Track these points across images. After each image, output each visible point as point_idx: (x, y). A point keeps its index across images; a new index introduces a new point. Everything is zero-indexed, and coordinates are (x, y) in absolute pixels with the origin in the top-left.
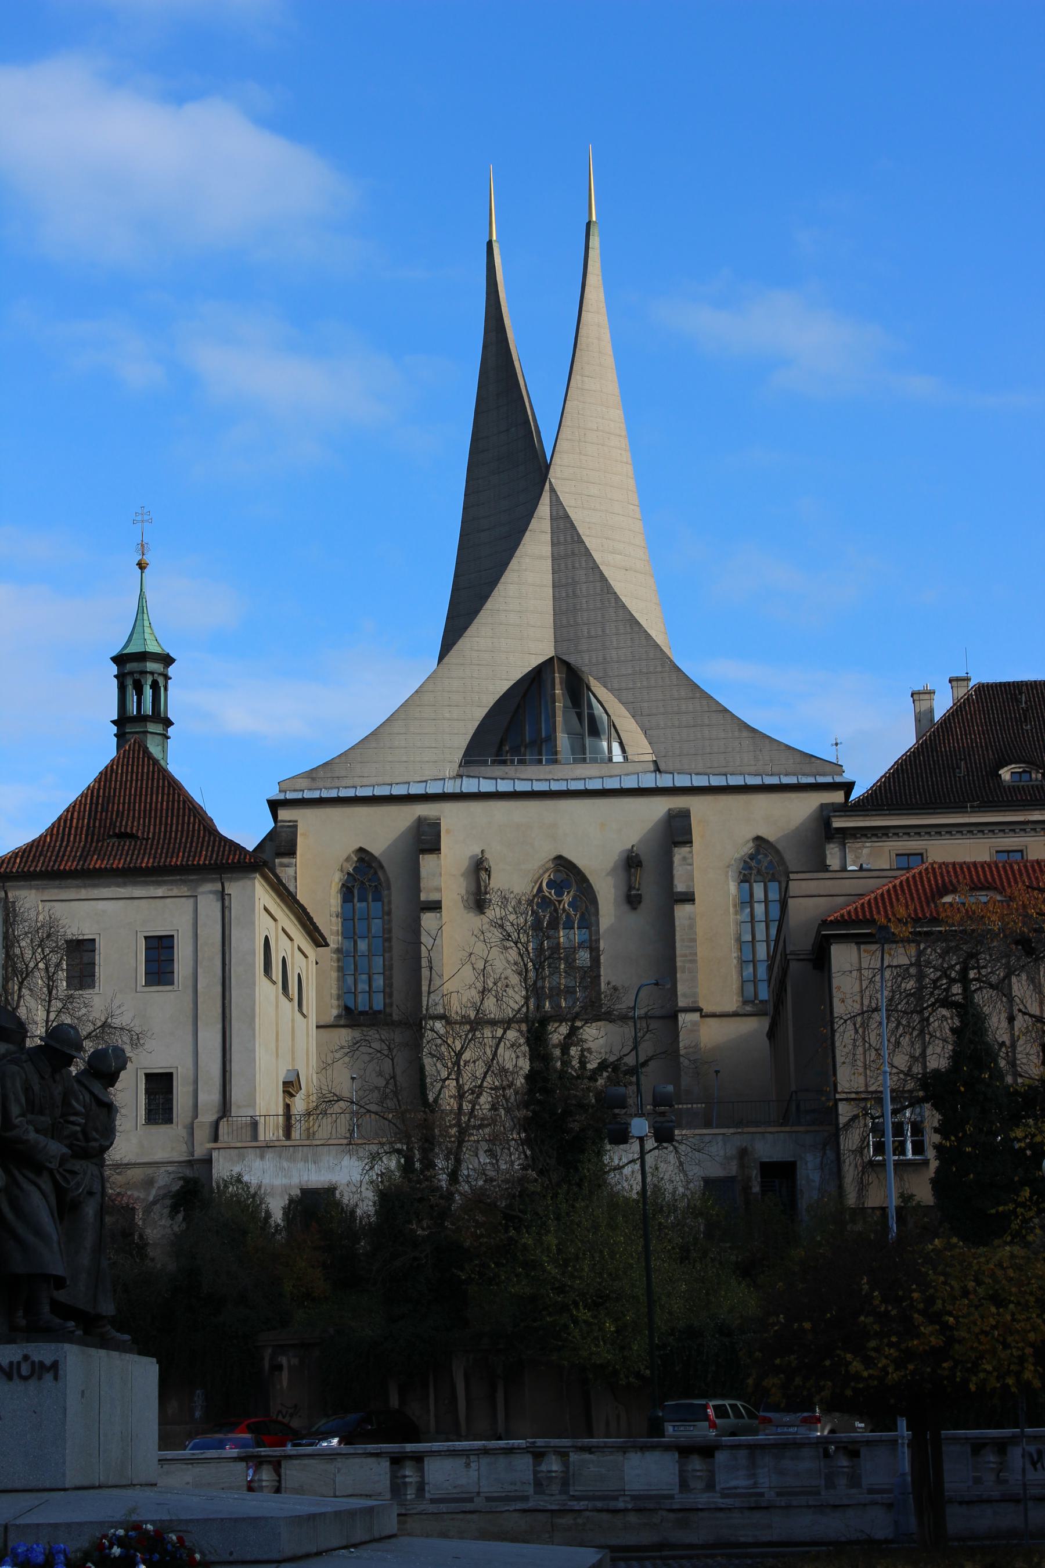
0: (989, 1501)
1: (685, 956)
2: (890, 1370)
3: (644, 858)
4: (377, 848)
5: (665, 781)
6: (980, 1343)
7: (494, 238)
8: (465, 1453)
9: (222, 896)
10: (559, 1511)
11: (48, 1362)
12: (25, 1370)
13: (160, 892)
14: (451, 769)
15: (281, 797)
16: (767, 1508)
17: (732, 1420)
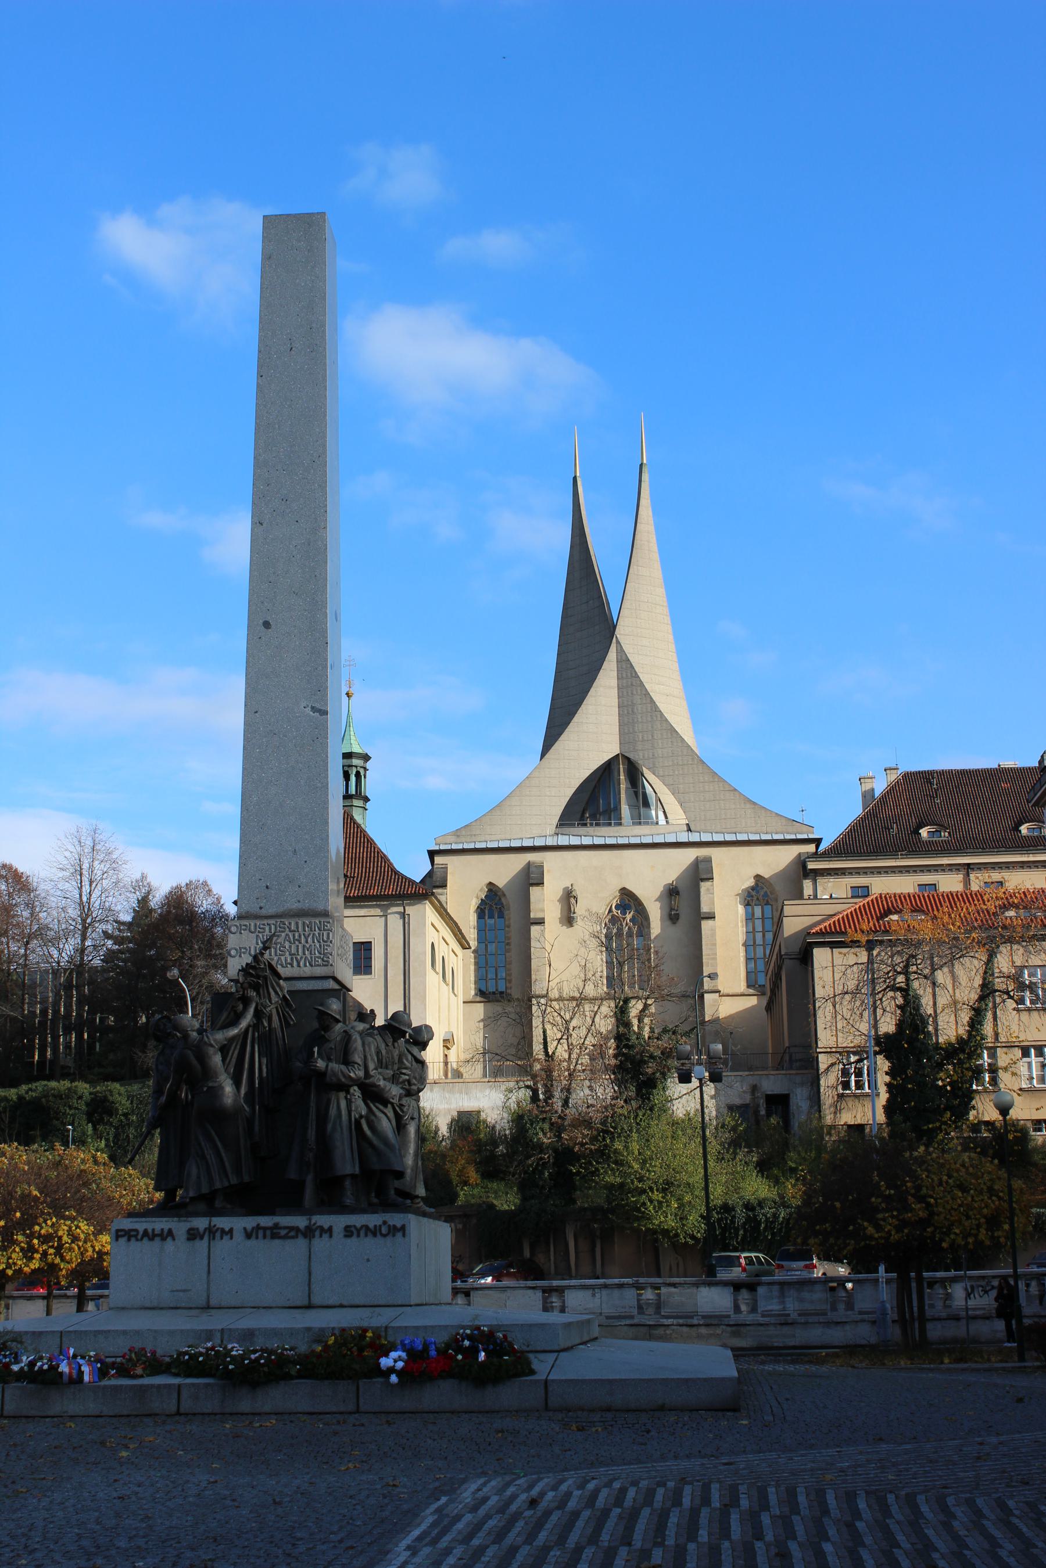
0: (939, 1319)
1: (709, 955)
2: (893, 1233)
3: (680, 889)
4: (501, 883)
5: (694, 837)
6: (952, 1216)
7: (578, 475)
9: (403, 915)
10: (655, 1325)
11: (399, 1226)
12: (384, 1230)
13: (362, 912)
14: (551, 829)
15: (437, 848)
16: (792, 1324)
17: (757, 1266)
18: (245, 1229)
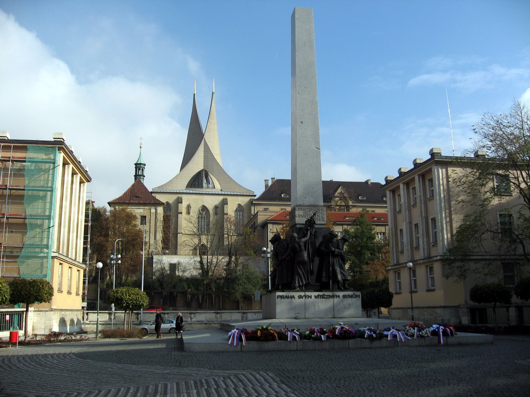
5: (223, 193)
8: (255, 312)
11: (358, 295)
12: (354, 296)
15: (153, 191)
18: (315, 296)
